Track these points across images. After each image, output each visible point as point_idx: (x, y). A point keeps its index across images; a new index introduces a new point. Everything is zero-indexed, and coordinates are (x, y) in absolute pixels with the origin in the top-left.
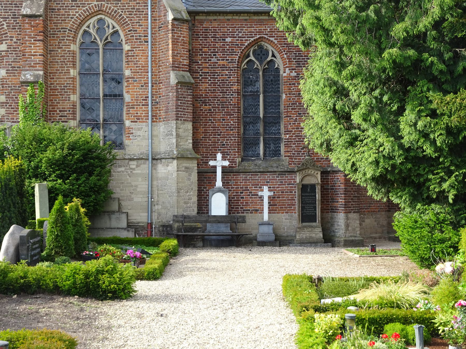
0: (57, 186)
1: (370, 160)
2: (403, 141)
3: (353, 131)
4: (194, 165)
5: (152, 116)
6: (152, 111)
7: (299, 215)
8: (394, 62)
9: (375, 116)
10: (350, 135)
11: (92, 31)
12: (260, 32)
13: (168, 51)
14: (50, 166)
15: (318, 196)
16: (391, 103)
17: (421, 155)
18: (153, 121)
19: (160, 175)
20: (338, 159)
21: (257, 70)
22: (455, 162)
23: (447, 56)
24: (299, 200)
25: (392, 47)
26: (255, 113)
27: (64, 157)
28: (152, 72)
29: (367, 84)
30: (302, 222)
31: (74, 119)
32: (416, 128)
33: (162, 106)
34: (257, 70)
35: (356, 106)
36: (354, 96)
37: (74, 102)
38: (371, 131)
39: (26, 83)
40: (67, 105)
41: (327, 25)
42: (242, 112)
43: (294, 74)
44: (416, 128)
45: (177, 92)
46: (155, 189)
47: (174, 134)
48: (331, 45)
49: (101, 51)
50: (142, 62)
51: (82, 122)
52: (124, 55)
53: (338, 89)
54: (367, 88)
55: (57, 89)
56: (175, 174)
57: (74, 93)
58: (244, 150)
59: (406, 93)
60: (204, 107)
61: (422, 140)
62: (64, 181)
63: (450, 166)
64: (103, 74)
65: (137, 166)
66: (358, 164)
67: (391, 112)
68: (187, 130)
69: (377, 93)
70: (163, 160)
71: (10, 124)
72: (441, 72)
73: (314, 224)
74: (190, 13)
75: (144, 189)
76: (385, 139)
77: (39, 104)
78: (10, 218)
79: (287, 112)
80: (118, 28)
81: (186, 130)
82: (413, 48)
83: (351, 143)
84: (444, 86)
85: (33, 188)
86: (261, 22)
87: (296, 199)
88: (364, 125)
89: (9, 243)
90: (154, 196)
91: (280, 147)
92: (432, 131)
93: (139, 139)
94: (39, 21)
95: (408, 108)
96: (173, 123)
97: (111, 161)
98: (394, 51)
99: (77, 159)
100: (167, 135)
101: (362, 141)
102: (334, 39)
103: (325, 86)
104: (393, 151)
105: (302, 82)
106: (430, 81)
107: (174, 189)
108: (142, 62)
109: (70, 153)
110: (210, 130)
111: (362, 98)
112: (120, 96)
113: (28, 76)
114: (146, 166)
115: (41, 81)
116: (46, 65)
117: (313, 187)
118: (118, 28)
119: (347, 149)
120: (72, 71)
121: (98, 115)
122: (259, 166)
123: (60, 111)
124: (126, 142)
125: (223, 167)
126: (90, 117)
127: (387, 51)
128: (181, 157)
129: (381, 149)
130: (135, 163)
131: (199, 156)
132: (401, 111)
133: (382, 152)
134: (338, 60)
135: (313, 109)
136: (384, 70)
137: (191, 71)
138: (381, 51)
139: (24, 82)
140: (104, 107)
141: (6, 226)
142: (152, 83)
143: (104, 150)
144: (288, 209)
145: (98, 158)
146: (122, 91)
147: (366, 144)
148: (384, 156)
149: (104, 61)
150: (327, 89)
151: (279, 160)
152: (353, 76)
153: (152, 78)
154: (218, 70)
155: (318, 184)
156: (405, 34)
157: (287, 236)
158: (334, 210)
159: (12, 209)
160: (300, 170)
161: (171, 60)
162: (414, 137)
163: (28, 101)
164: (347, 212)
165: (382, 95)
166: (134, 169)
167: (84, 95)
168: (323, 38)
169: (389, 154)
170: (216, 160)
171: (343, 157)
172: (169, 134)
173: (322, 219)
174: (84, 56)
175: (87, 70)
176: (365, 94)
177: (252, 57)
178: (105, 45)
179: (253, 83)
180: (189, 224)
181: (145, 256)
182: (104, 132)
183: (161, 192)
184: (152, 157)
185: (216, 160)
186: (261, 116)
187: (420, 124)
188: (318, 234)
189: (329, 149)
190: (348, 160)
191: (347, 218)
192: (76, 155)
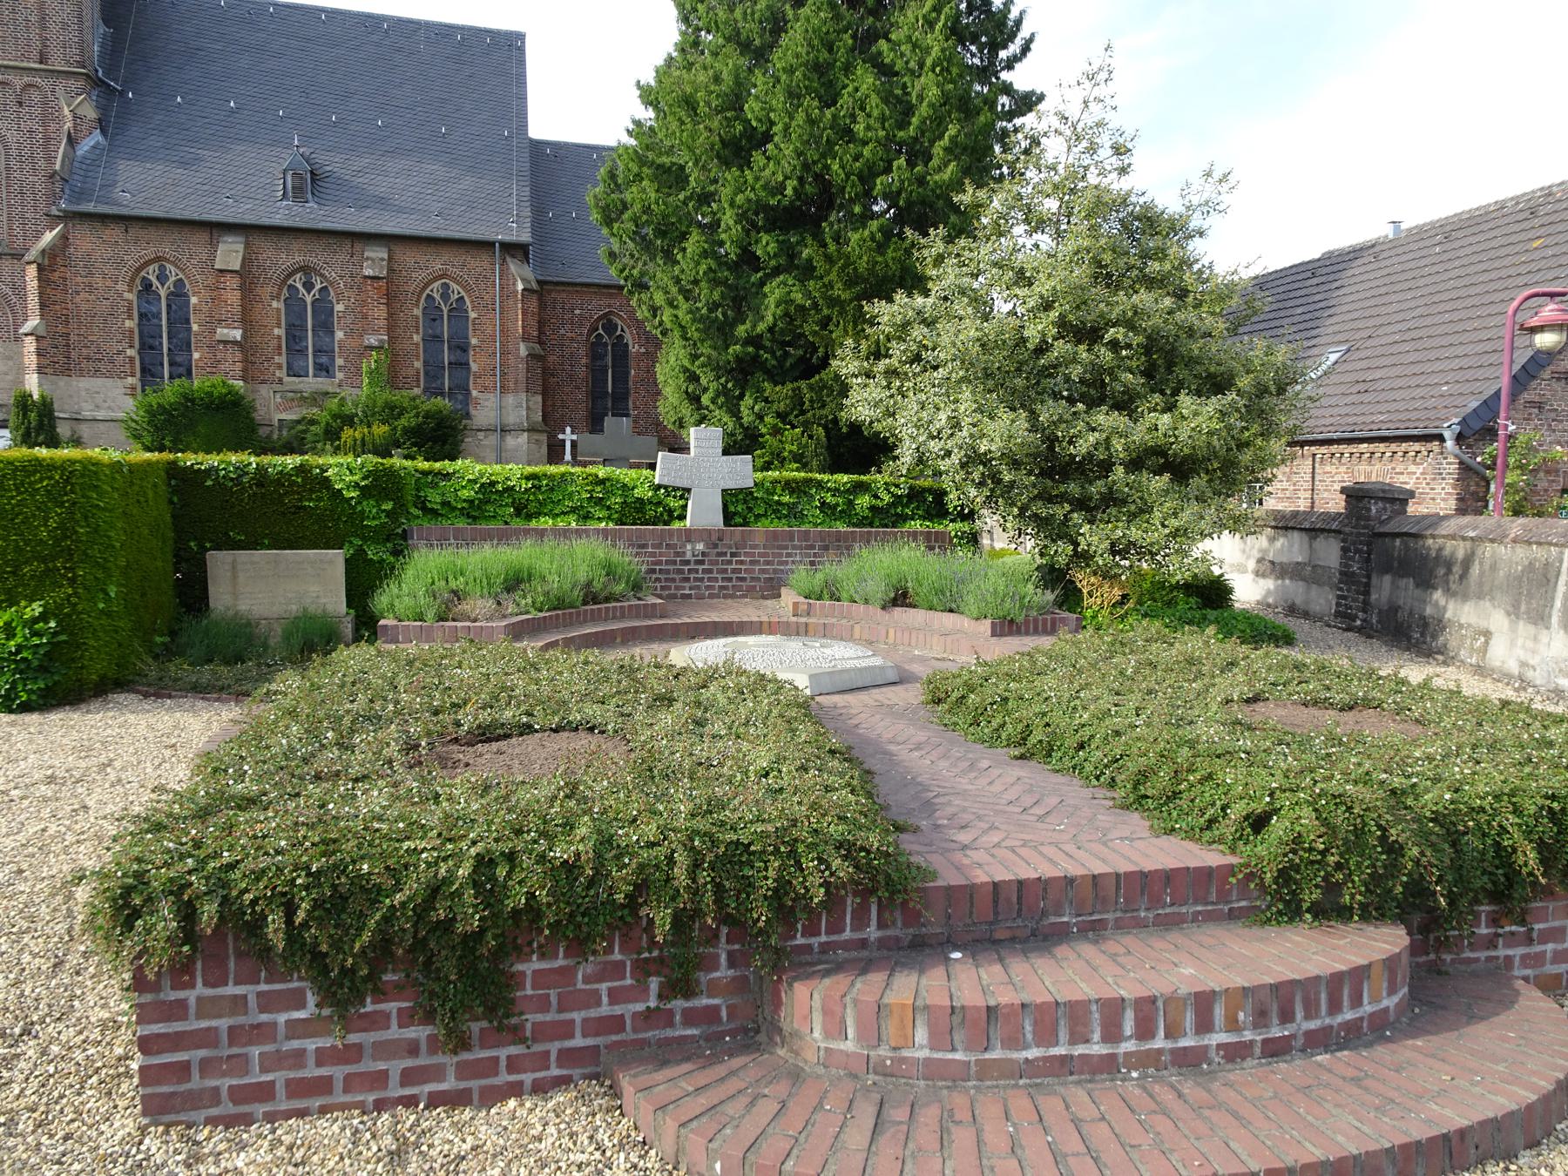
4: (544, 438)
9: (721, 400)
11: (437, 296)
12: (609, 306)
21: (606, 344)
23: (778, 354)
31: (418, 386)
33: (511, 377)
34: (606, 344)
35: (705, 390)
36: (704, 381)
38: (717, 412)
39: (372, 348)
40: (411, 372)
41: (683, 323)
48: (687, 339)
50: (489, 331)
51: (426, 390)
57: (418, 360)
68: (536, 403)
69: (723, 380)
74: (539, 282)
77: (384, 370)
80: (463, 293)
81: (536, 403)
86: (611, 295)
88: (712, 407)
94: (382, 283)
95: (748, 394)
96: (523, 396)
98: (738, 347)
106: (765, 373)
108: (489, 331)
110: (559, 403)
115: (386, 346)
116: (391, 329)
118: (463, 293)
120: (415, 336)
124: (473, 412)
128: (532, 430)
132: (741, 397)
135: (668, 391)
136: (729, 362)
138: (727, 348)
145: (450, 427)
150: (681, 375)
152: (703, 365)
154: (567, 343)
165: (727, 382)
172: (519, 406)
177: (601, 331)
178: (450, 311)
179: (603, 356)
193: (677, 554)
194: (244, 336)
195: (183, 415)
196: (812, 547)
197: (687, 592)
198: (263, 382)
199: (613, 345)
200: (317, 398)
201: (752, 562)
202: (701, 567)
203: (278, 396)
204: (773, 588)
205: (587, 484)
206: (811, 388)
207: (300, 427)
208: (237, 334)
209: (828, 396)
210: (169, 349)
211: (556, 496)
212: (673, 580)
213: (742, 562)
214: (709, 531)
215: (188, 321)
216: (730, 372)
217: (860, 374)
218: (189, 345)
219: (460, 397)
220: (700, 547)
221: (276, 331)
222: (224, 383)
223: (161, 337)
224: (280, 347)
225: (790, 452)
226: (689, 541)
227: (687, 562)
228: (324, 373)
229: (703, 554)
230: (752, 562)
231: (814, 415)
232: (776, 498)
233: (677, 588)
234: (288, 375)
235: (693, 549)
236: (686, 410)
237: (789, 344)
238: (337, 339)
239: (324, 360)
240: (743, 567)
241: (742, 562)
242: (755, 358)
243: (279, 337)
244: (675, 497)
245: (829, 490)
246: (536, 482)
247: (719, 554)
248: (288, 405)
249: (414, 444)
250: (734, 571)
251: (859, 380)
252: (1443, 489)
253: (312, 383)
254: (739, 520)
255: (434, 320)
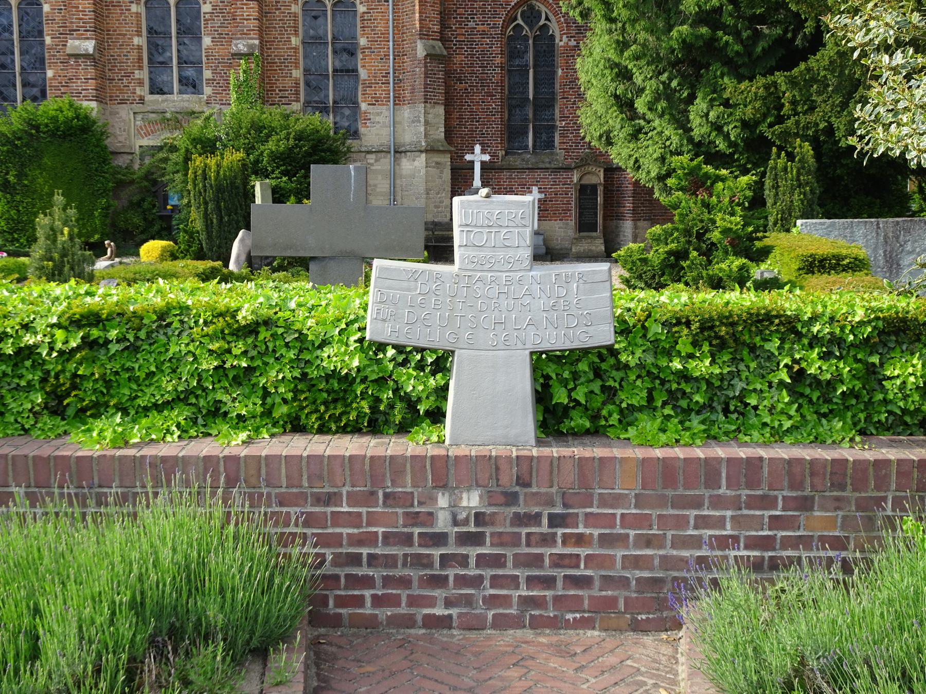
0: (282, 184)
1: (655, 156)
2: (692, 134)
3: (637, 121)
4: (446, 159)
5: (395, 97)
6: (394, 90)
7: (576, 223)
8: (684, 41)
10: (634, 126)
13: (414, 13)
14: (274, 160)
15: (600, 200)
16: (681, 90)
17: (713, 151)
18: (395, 104)
19: (404, 172)
20: (619, 154)
22: (752, 159)
23: (745, 35)
24: (576, 204)
25: (682, 24)
26: (523, 93)
27: (290, 149)
28: (394, 41)
29: (653, 67)
30: (580, 232)
31: (298, 101)
32: (707, 119)
33: (407, 85)
35: (641, 90)
36: (638, 79)
37: (296, 79)
38: (657, 123)
39: (239, 55)
40: (289, 83)
42: (507, 92)
43: (573, 43)
44: (707, 119)
45: (426, 67)
46: (398, 189)
47: (422, 120)
48: (612, 21)
49: (329, 13)
51: (307, 104)
52: (358, 19)
53: (620, 71)
54: (654, 71)
55: (276, 63)
56: (423, 172)
57: (297, 67)
58: (509, 141)
59: (698, 76)
60: (458, 86)
61: (714, 134)
62: (290, 179)
63: (746, 163)
64: (333, 43)
65: (376, 161)
66: (641, 160)
67: (680, 100)
68: (438, 116)
69: (664, 77)
70: (408, 154)
71: (218, 106)
72: (737, 53)
73: (594, 234)
75: (384, 190)
76: (673, 132)
77: (254, 83)
78: (237, 222)
79: (564, 92)
81: (438, 116)
82: (707, 25)
83: (635, 136)
84: (741, 71)
85: (253, 187)
87: (573, 203)
88: (650, 116)
89: (239, 250)
90: (397, 198)
91: (554, 137)
92: (725, 123)
93: (378, 126)
95: (700, 95)
97: (345, 154)
98: (685, 28)
99: (305, 152)
100: (413, 122)
101: (646, 133)
102: (614, 15)
103: (606, 68)
104: (682, 145)
105: (579, 60)
106: (725, 64)
107: (422, 189)
109: (296, 145)
110: (467, 115)
111: (648, 84)
112: (352, 72)
113: (241, 47)
114: (387, 160)
115: (257, 52)
116: (262, 32)
117: (594, 187)
119: (629, 142)
120: (293, 39)
121: (327, 96)
122: (527, 161)
123: (280, 91)
124: (362, 130)
125: (483, 163)
126: (316, 98)
127: (676, 29)
128: (430, 150)
129: (668, 143)
130: (373, 156)
131: (453, 149)
132: (691, 99)
133: (669, 146)
134: (621, 39)
135: (591, 94)
137: (443, 39)
138: (670, 28)
139: (236, 54)
140: (334, 85)
141: (233, 231)
142: (394, 55)
143: (335, 140)
144: (561, 215)
145: (329, 150)
146: (357, 65)
147: (651, 138)
148: (671, 151)
149: (333, 26)
150: (607, 72)
151: (552, 154)
152: (637, 58)
153: (394, 49)
154: (477, 38)
155: (600, 184)
156: (697, 9)
157: (561, 249)
158: (620, 217)
159: (239, 211)
160: (579, 167)
161: (418, 25)
162: (705, 129)
163: (241, 78)
164: (635, 220)
165: (670, 79)
166: (372, 165)
167: (309, 70)
168: (603, 12)
169: (676, 150)
170: (473, 153)
171: (625, 152)
173: (604, 227)
174: (308, 19)
175: (312, 38)
176: (651, 78)
177: (520, 21)
179: (522, 53)
180: (440, 233)
181: (131, 499)
182: (334, 117)
183: (406, 193)
184: (395, 149)
185: (473, 153)
186: (531, 97)
187: (712, 115)
188: (599, 246)
189: (609, 143)
190: (630, 156)
191: (636, 227)
192: (304, 146)
193: (414, 519)
194: (99, 48)
195: (27, 145)
196: (767, 502)
197: (439, 611)
198: (123, 102)
199: (535, 38)
200: (176, 121)
201: (606, 540)
202: (473, 552)
203: (139, 117)
204: (662, 604)
205: (212, 337)
206: (793, 83)
207: (161, 155)
208: (89, 46)
209: (819, 93)
210: (22, 68)
211: (142, 364)
212: (405, 582)
213: (580, 540)
214: (494, 464)
215: (41, 33)
216: (673, 65)
217: (899, 44)
218: (42, 61)
219: (347, 112)
220: (472, 500)
221: (136, 41)
222: (71, 105)
223: (13, 53)
224: (140, 59)
225: (726, 231)
226: (444, 487)
227: (439, 539)
228: (191, 89)
229: (480, 518)
230: (606, 540)
231: (797, 123)
232: (677, 365)
233: (414, 601)
234: (152, 93)
235: (454, 506)
236: (615, 120)
237: (762, 19)
238: (204, 46)
239: (190, 72)
240: (583, 552)
241: (580, 540)
242: (711, 44)
243: (140, 48)
244: (420, 366)
245: (815, 341)
246: (95, 333)
247: (521, 520)
248: (149, 129)
249: (284, 173)
250: (559, 561)
251: (899, 59)
252: (455, 45)
253: (176, 101)
254: (580, 421)
255: (315, 18)
